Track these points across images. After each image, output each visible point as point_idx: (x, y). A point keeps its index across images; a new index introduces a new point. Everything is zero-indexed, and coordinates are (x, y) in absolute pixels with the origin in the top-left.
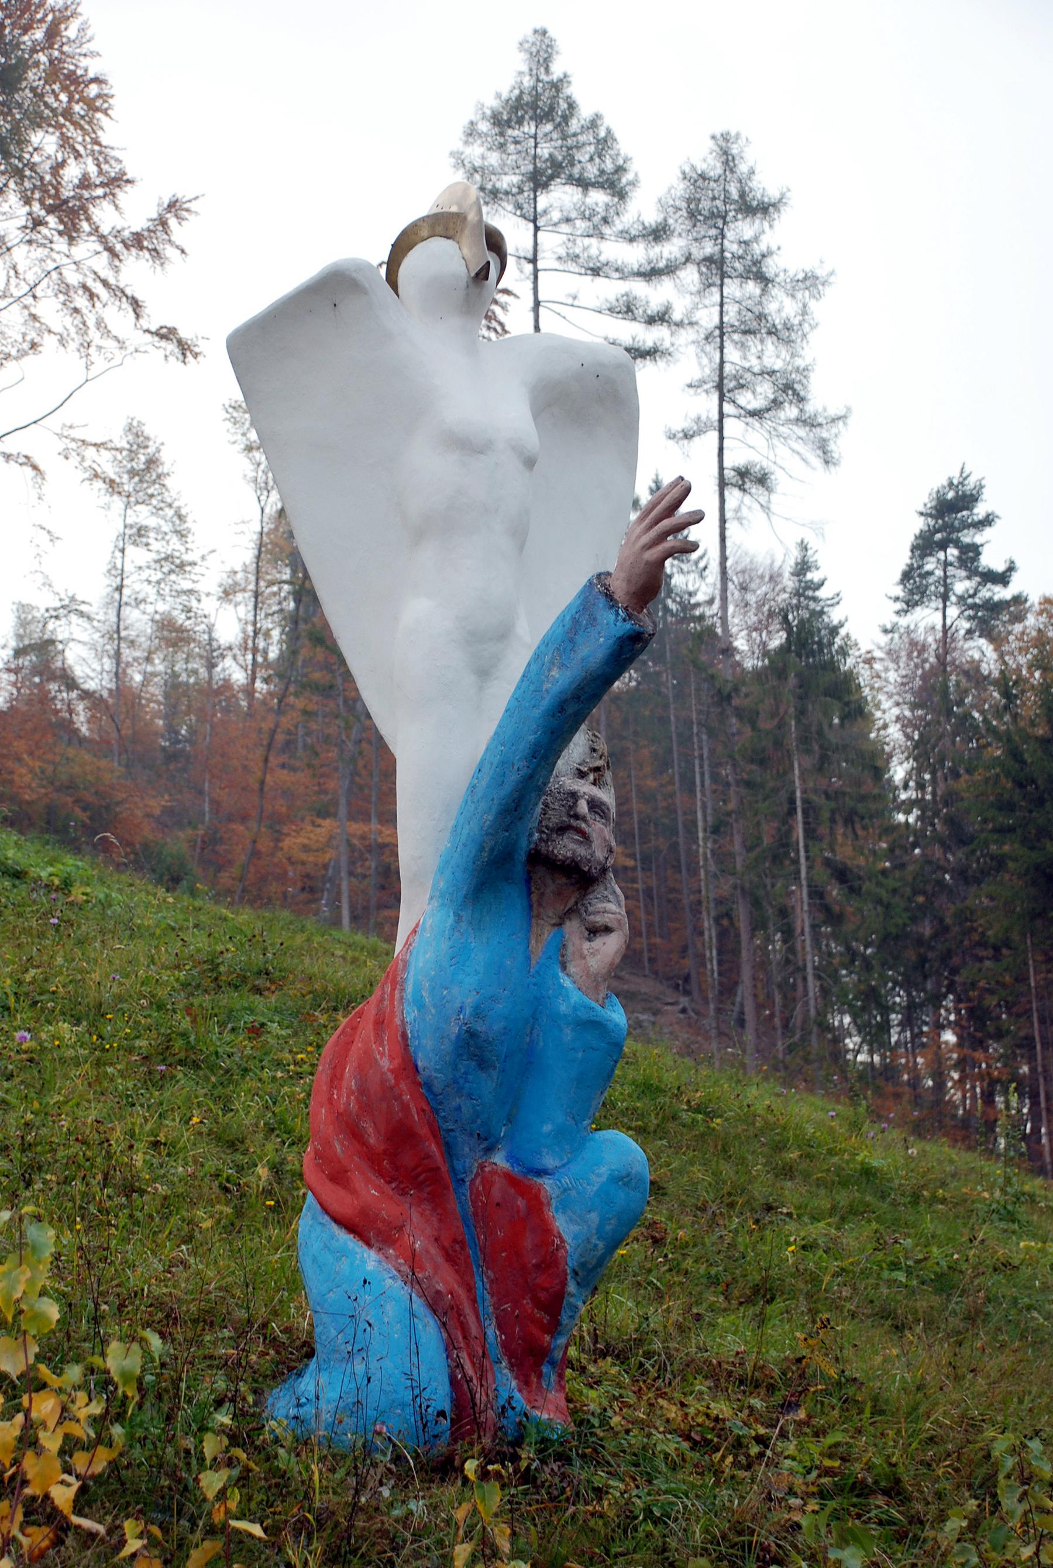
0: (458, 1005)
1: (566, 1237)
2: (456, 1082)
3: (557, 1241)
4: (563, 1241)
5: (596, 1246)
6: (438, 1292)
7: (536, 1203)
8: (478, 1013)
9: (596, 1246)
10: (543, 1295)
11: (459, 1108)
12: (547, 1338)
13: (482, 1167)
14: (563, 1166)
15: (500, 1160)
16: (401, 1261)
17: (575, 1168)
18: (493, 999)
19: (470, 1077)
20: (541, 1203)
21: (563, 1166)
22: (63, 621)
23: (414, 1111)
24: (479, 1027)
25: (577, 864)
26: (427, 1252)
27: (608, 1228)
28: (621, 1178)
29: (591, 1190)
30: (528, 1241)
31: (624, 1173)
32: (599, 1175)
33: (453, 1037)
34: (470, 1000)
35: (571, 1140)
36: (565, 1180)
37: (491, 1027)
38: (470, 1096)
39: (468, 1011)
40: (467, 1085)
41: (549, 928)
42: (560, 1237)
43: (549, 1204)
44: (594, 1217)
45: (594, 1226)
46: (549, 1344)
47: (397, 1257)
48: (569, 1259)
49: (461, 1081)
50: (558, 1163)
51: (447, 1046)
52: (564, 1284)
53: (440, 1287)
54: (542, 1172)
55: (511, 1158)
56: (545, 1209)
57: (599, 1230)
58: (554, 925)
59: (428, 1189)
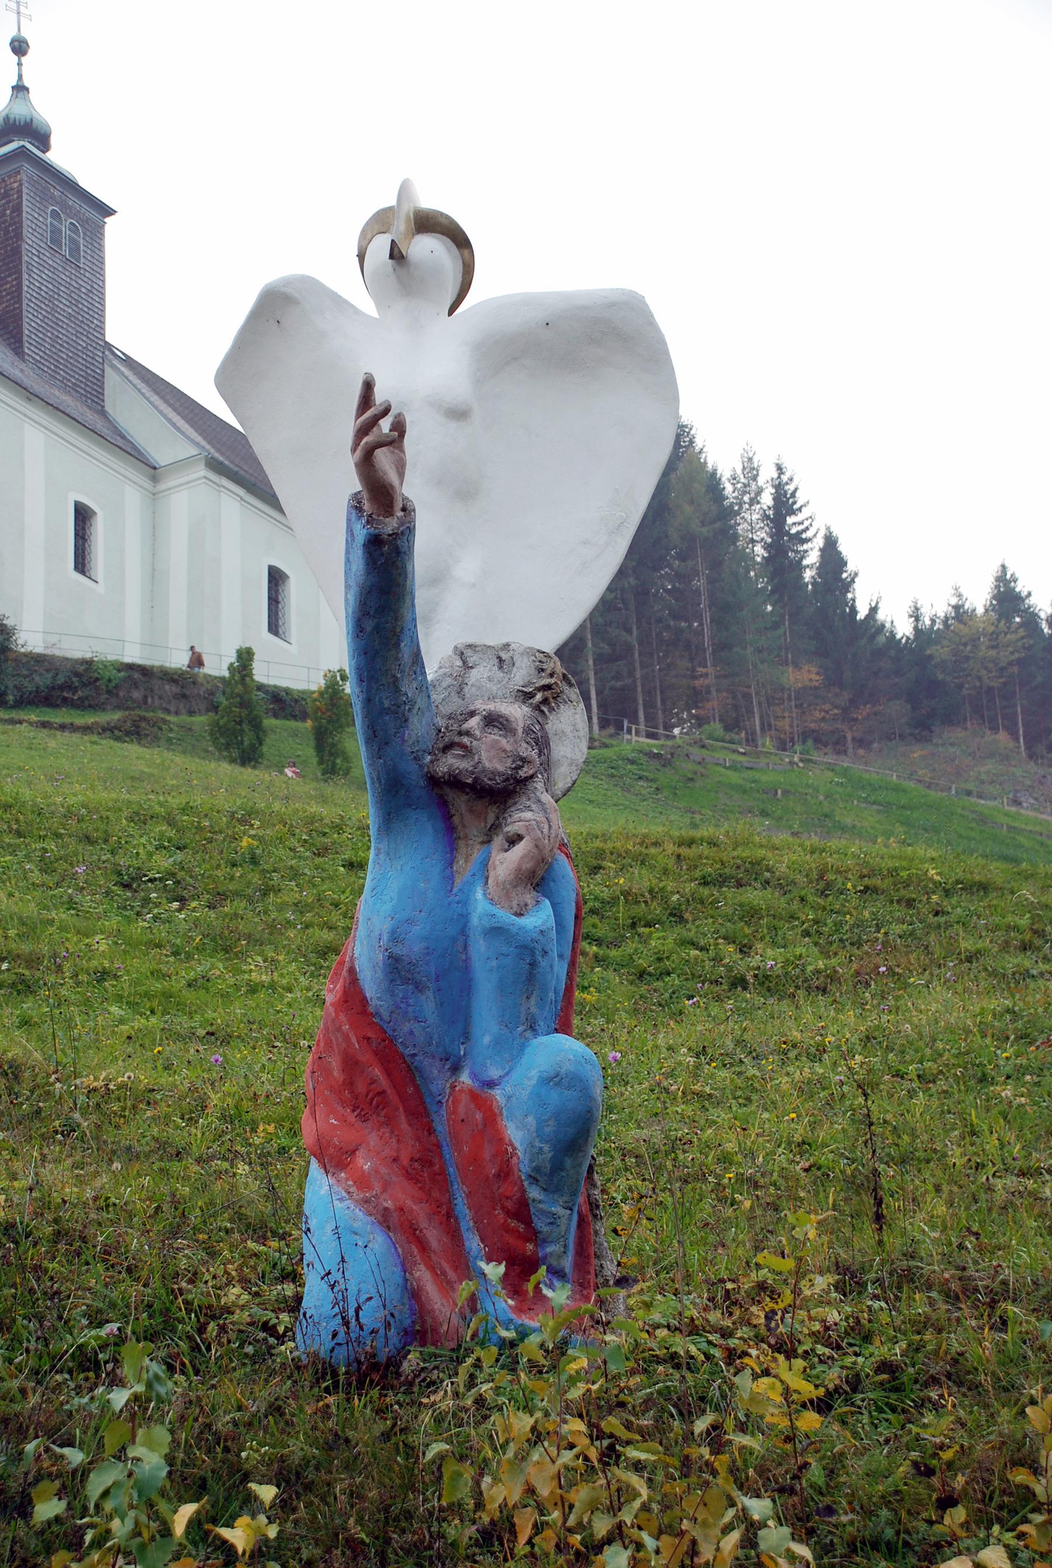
0: (377, 933)
1: (517, 1144)
2: (398, 1007)
3: (510, 1149)
4: (515, 1149)
5: (541, 1149)
6: (386, 1209)
7: (491, 1117)
8: (395, 937)
9: (541, 1149)
10: (509, 1204)
11: (411, 1033)
12: (530, 1247)
13: (453, 1087)
14: (507, 1074)
15: (465, 1078)
16: (351, 1183)
17: (515, 1076)
18: (409, 921)
19: (411, 1001)
20: (494, 1115)
21: (507, 1074)
22: (484, 706)
23: (354, 1040)
24: (398, 950)
25: (455, 777)
26: (377, 1172)
27: (547, 1130)
28: (551, 1079)
29: (525, 1094)
30: (487, 1153)
31: (552, 1073)
32: (530, 1079)
33: (381, 964)
34: (386, 926)
35: (511, 1048)
36: (508, 1089)
37: (413, 948)
38: (417, 1020)
39: (385, 937)
40: (410, 1009)
41: (478, 846)
42: (512, 1145)
43: (501, 1114)
44: (531, 1120)
45: (533, 1129)
46: (536, 1253)
47: (347, 1179)
48: (521, 1166)
49: (403, 1006)
50: (501, 1073)
51: (380, 975)
52: (523, 1191)
53: (389, 1204)
54: (491, 1084)
55: (474, 1076)
56: (499, 1119)
57: (538, 1130)
58: (483, 843)
59: (383, 1113)
